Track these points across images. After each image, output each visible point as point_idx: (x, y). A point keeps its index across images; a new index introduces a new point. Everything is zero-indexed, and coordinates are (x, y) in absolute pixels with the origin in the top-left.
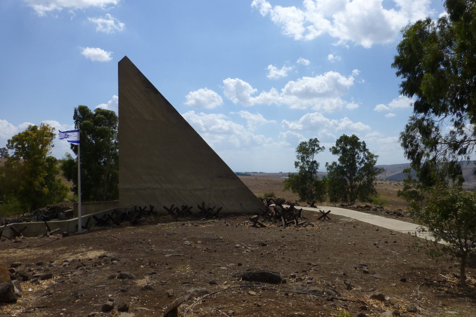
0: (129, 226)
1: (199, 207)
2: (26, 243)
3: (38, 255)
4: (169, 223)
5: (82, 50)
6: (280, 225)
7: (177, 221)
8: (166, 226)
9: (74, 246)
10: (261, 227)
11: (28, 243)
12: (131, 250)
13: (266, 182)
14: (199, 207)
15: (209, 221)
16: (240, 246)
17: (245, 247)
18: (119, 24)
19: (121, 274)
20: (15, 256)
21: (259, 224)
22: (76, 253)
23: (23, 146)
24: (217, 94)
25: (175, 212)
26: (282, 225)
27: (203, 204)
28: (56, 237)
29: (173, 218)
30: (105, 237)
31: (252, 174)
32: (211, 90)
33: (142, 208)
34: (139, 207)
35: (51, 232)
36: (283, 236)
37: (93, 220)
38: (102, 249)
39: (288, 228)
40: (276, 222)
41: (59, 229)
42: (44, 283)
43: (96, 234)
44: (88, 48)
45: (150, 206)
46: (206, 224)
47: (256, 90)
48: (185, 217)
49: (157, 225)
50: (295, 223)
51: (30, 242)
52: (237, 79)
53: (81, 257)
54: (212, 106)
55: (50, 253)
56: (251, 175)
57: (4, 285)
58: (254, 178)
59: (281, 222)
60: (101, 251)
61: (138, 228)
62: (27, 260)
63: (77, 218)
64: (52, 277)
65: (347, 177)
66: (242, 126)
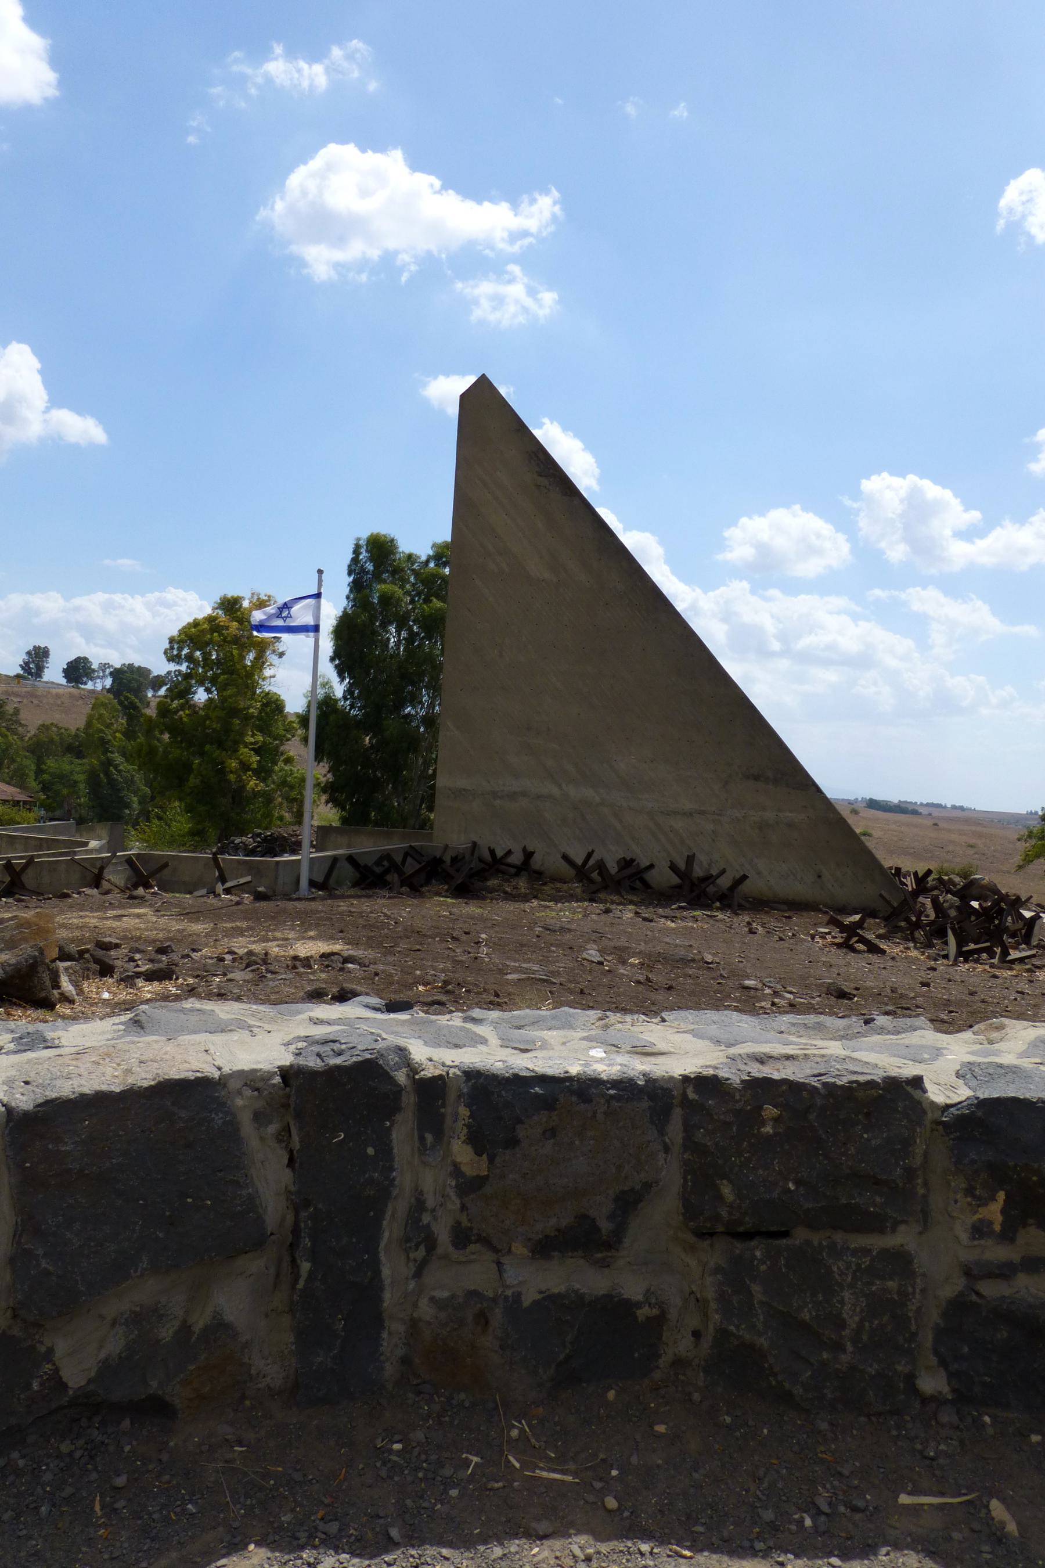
0: (443, 897)
1: (673, 867)
2: (156, 903)
3: (169, 931)
4: (566, 904)
5: (425, 385)
6: (939, 955)
7: (592, 900)
8: (554, 910)
9: (270, 923)
10: (869, 951)
11: (159, 904)
12: (418, 953)
13: (972, 841)
14: (673, 867)
15: (697, 913)
16: (760, 986)
17: (775, 992)
18: (540, 296)
19: (342, 989)
20: (114, 926)
21: (863, 940)
22: (268, 940)
23: (206, 656)
24: (830, 527)
25: (595, 875)
26: (946, 957)
27: (690, 859)
28: (235, 898)
29: (583, 892)
30: (361, 913)
31: (924, 811)
32: (811, 515)
33: (500, 853)
34: (489, 848)
35: (228, 885)
36: (925, 980)
37: (347, 871)
38: (341, 939)
39: (963, 967)
40: (930, 945)
41: (248, 879)
42: (146, 989)
43: (342, 904)
44: (441, 378)
45: (524, 849)
46: (683, 918)
47: (975, 515)
48: (624, 893)
49: (529, 904)
50: (997, 957)
51: (164, 903)
52: (912, 478)
53: (277, 949)
54: (810, 568)
55: (202, 930)
56: (920, 814)
57: (22, 954)
58: (930, 823)
59: (946, 947)
60: (334, 944)
61: (466, 903)
62: (140, 938)
63: (300, 857)
64: (174, 977)
66: (909, 643)
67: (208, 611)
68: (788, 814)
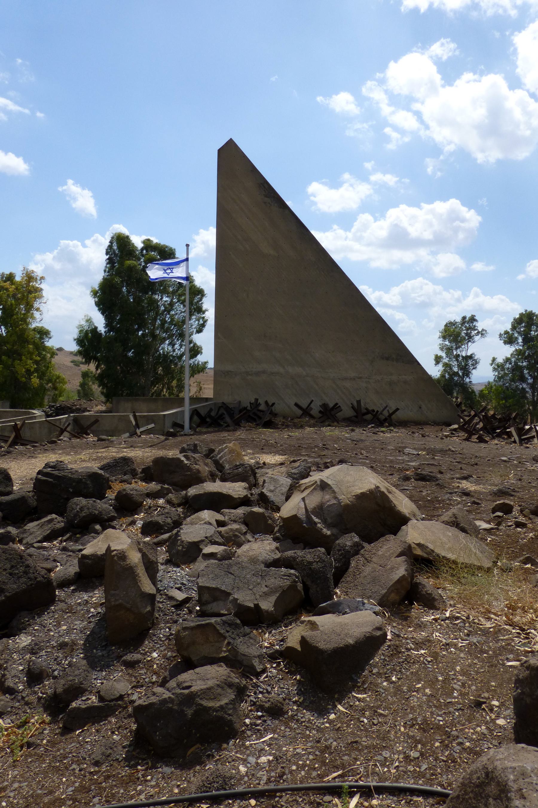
27: (359, 402)
41: (153, 425)
65: (528, 384)
67: (39, 275)
68: (404, 377)
